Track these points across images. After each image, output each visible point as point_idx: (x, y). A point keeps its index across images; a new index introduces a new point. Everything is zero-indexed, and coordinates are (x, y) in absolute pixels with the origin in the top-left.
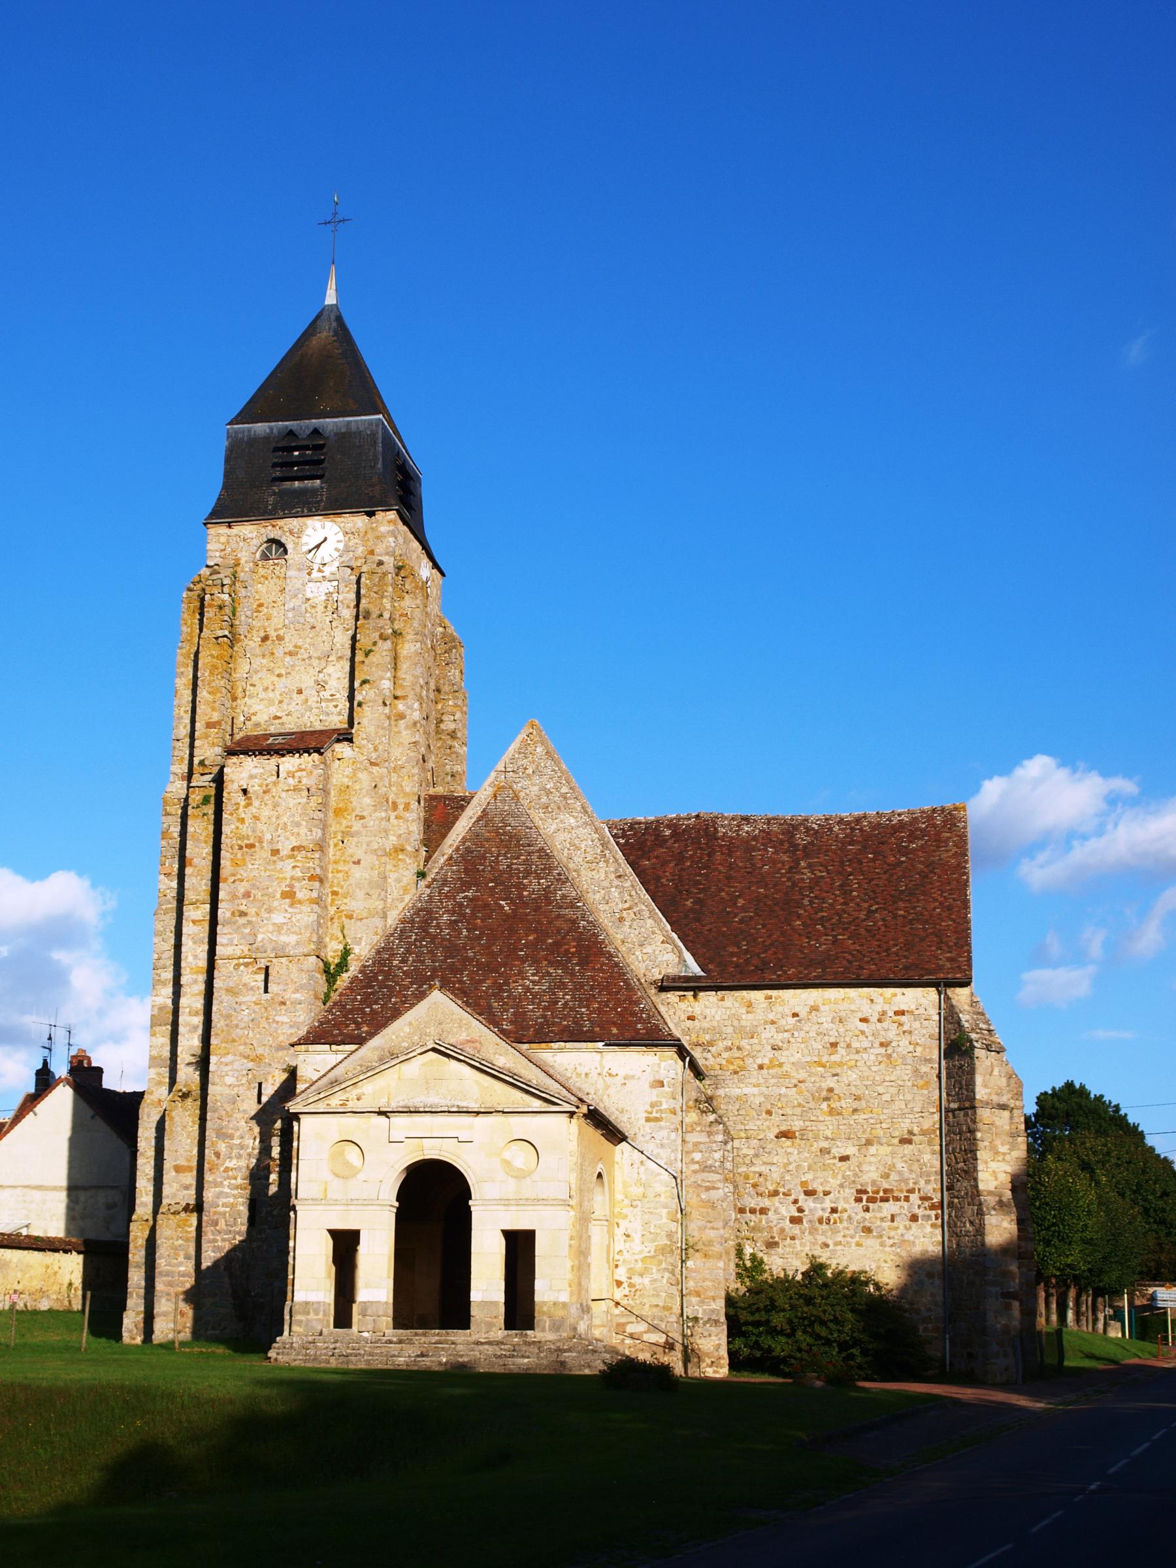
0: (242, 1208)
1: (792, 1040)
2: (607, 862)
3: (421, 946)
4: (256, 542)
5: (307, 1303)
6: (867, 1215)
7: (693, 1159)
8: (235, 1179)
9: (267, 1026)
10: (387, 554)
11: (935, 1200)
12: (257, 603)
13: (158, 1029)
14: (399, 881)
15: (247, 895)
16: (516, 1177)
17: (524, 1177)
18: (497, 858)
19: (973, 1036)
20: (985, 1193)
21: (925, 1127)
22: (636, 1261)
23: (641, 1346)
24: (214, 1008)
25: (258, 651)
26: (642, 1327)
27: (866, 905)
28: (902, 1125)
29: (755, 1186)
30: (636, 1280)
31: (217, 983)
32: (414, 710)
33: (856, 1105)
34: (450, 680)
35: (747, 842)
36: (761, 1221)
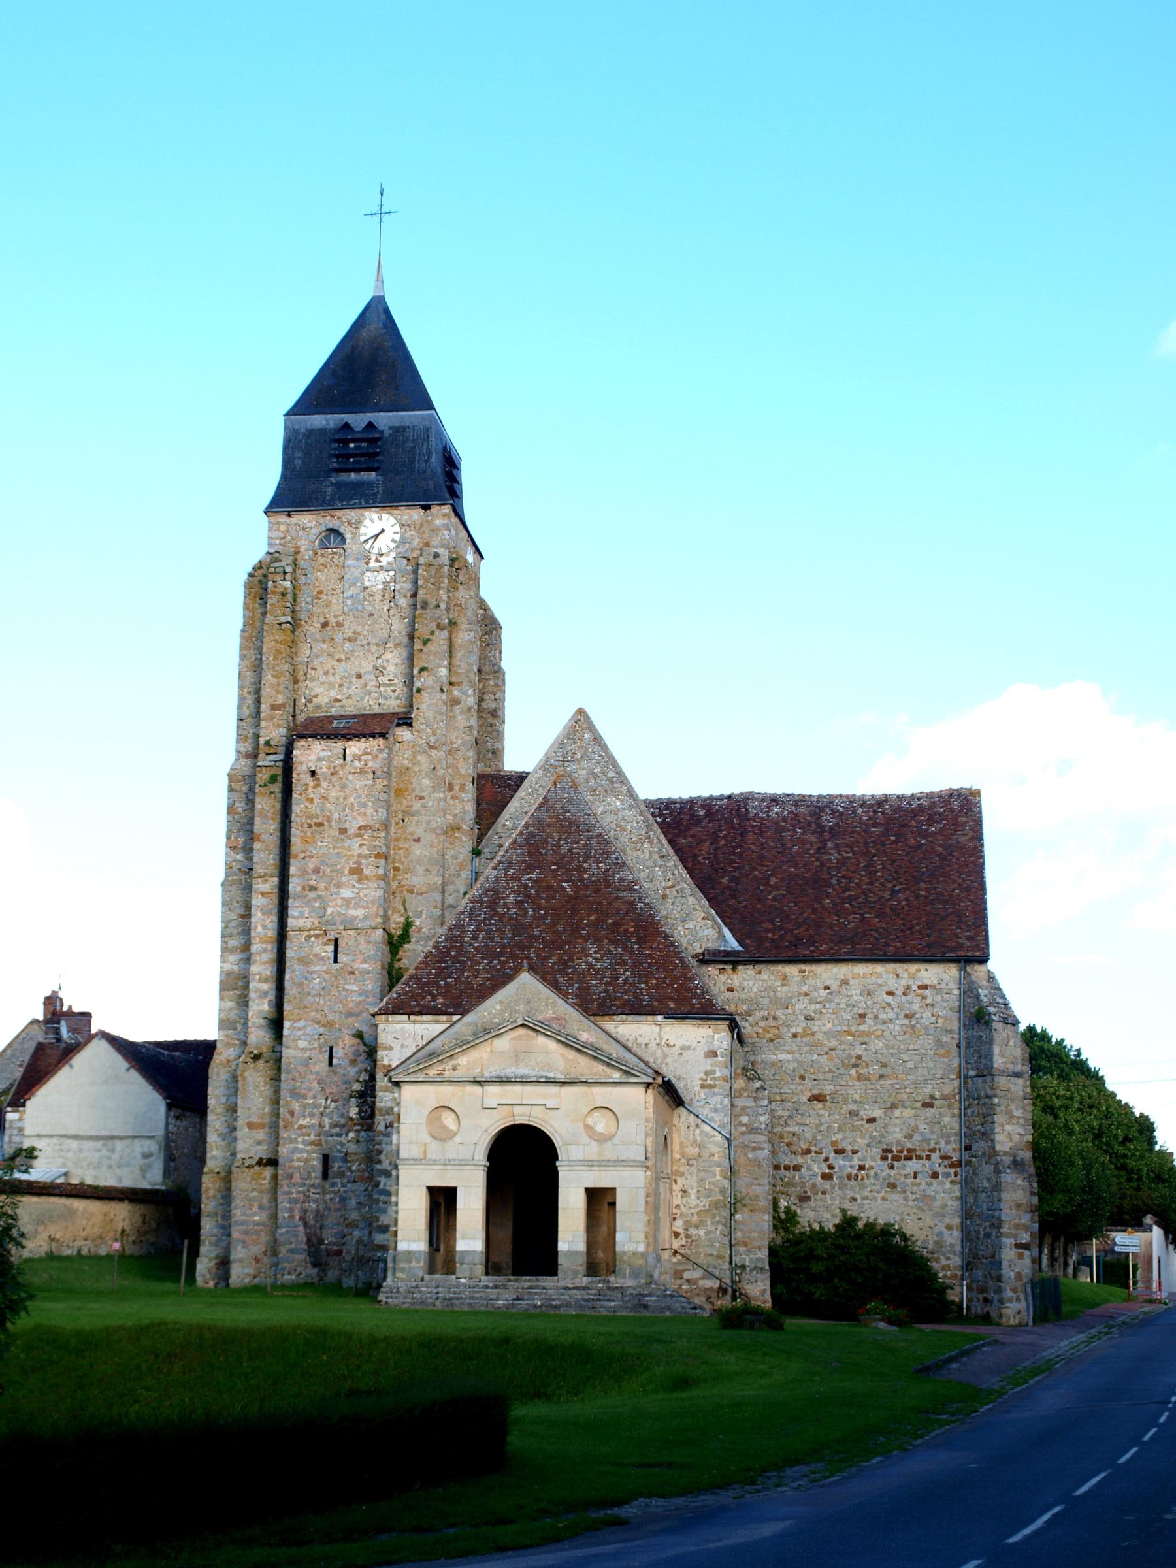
0: (315, 1163)
1: (824, 1011)
2: (651, 842)
3: (491, 924)
4: (314, 531)
5: (409, 1252)
6: (892, 1172)
7: (740, 1122)
8: (309, 1135)
9: (337, 994)
10: (442, 546)
11: (954, 1159)
12: (317, 590)
13: (225, 993)
14: (455, 857)
15: (317, 871)
16: (598, 1141)
17: (606, 1141)
18: (558, 843)
19: (992, 1010)
20: (1001, 1153)
21: (946, 1092)
22: (692, 1214)
23: (697, 1291)
24: (287, 977)
25: (318, 636)
26: (696, 1274)
27: (890, 885)
28: (925, 1090)
29: (789, 1145)
30: (693, 1231)
31: (289, 953)
32: (468, 696)
33: (883, 1071)
34: (490, 661)
35: (777, 823)
36: (794, 1177)
